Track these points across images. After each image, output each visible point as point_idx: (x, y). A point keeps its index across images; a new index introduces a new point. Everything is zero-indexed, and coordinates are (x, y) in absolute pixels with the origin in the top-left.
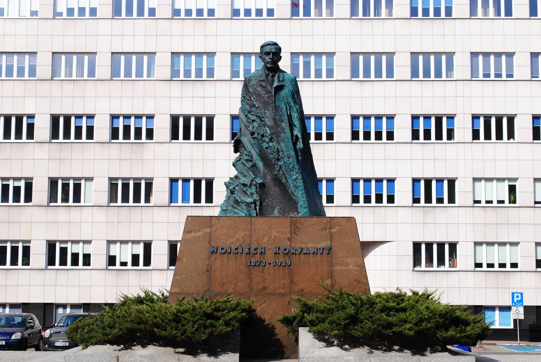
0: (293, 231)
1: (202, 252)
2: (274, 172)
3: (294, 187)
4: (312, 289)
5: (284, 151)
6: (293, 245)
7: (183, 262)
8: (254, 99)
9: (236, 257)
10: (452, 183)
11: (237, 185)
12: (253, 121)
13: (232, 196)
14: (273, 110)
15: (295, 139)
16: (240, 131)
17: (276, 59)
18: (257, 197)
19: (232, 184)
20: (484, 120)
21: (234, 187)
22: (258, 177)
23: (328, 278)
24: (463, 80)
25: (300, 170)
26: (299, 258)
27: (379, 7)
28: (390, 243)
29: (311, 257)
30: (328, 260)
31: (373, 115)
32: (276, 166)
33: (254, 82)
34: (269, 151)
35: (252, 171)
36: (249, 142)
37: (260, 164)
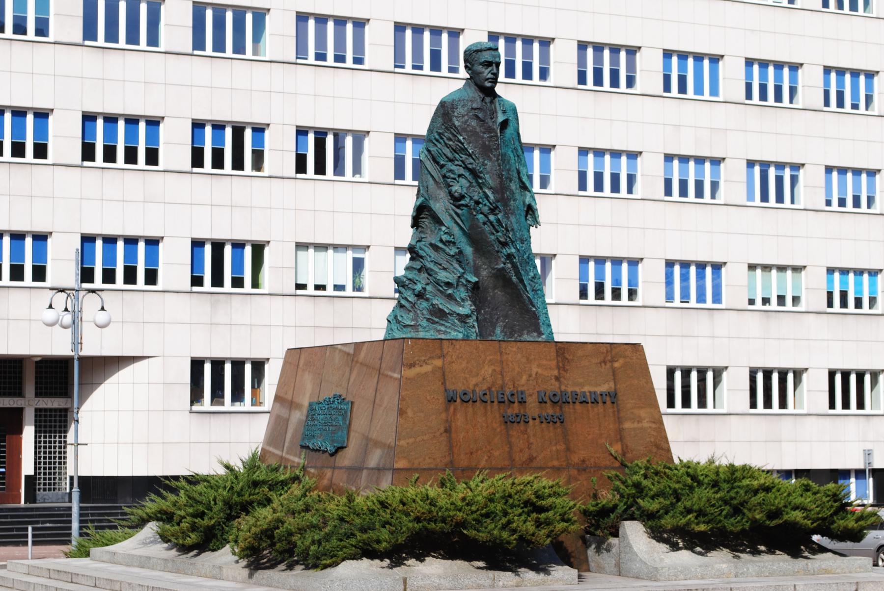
0: (561, 365)
1: (434, 400)
2: (496, 265)
4: (596, 459)
6: (563, 388)
8: (463, 138)
9: (485, 408)
10: (258, 249)
23: (617, 442)
24: (284, 63)
26: (574, 409)
28: (150, 359)
31: (31, 109)
35: (457, 261)
37: (468, 250)
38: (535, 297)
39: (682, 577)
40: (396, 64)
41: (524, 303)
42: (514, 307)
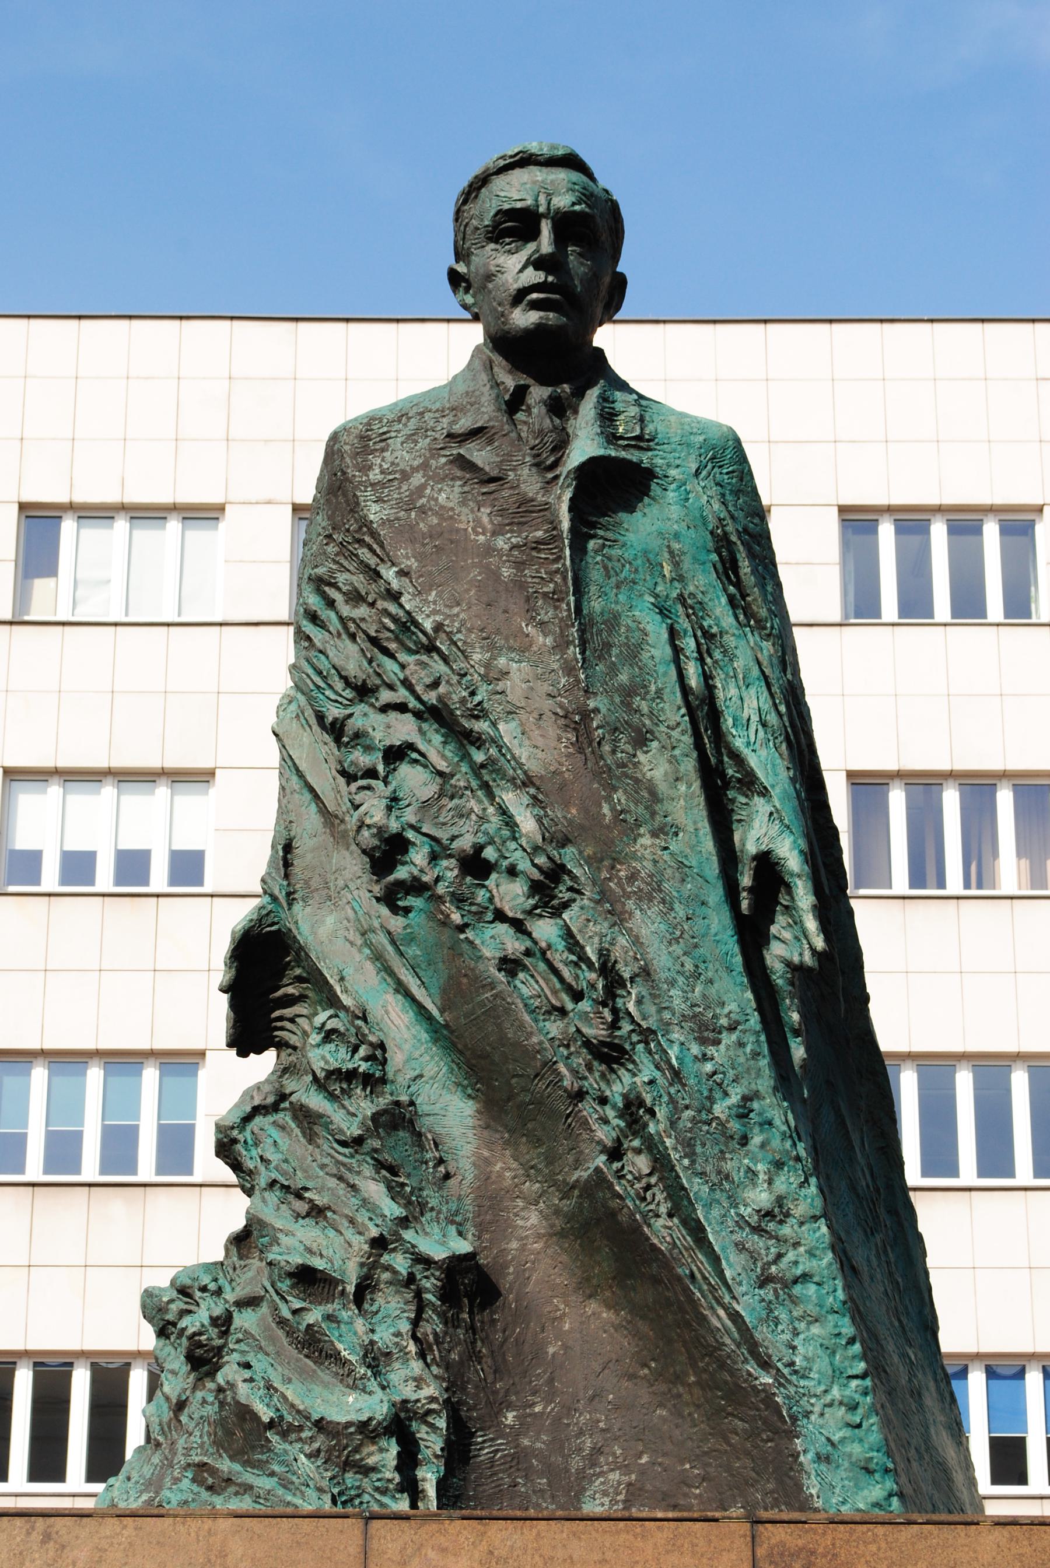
2: (577, 1164)
3: (761, 1287)
5: (663, 975)
11: (251, 1302)
12: (395, 754)
13: (199, 1394)
15: (750, 890)
16: (287, 864)
17: (582, 269)
18: (419, 1382)
19: (204, 1289)
21: (218, 1311)
22: (428, 1215)
25: (801, 1146)
27: (986, 848)
32: (588, 1109)
33: (398, 454)
34: (525, 991)
35: (380, 1165)
36: (359, 941)
38: (782, 1314)
40: (1005, 799)
41: (714, 1351)
42: (678, 1378)
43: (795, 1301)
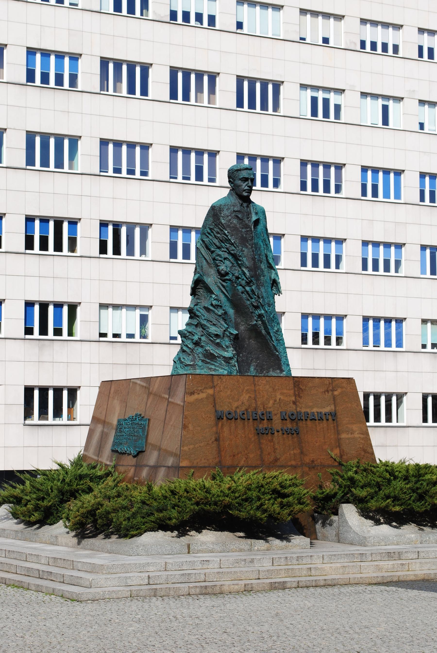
0: (297, 393)
2: (251, 322)
7: (189, 430)
8: (228, 232)
9: (244, 424)
12: (225, 259)
14: (252, 247)
20: (114, 229)
23: (336, 448)
26: (306, 424)
29: (317, 424)
30: (334, 427)
35: (223, 319)
37: (231, 312)
38: (279, 345)
39: (383, 543)
43: (280, 343)
